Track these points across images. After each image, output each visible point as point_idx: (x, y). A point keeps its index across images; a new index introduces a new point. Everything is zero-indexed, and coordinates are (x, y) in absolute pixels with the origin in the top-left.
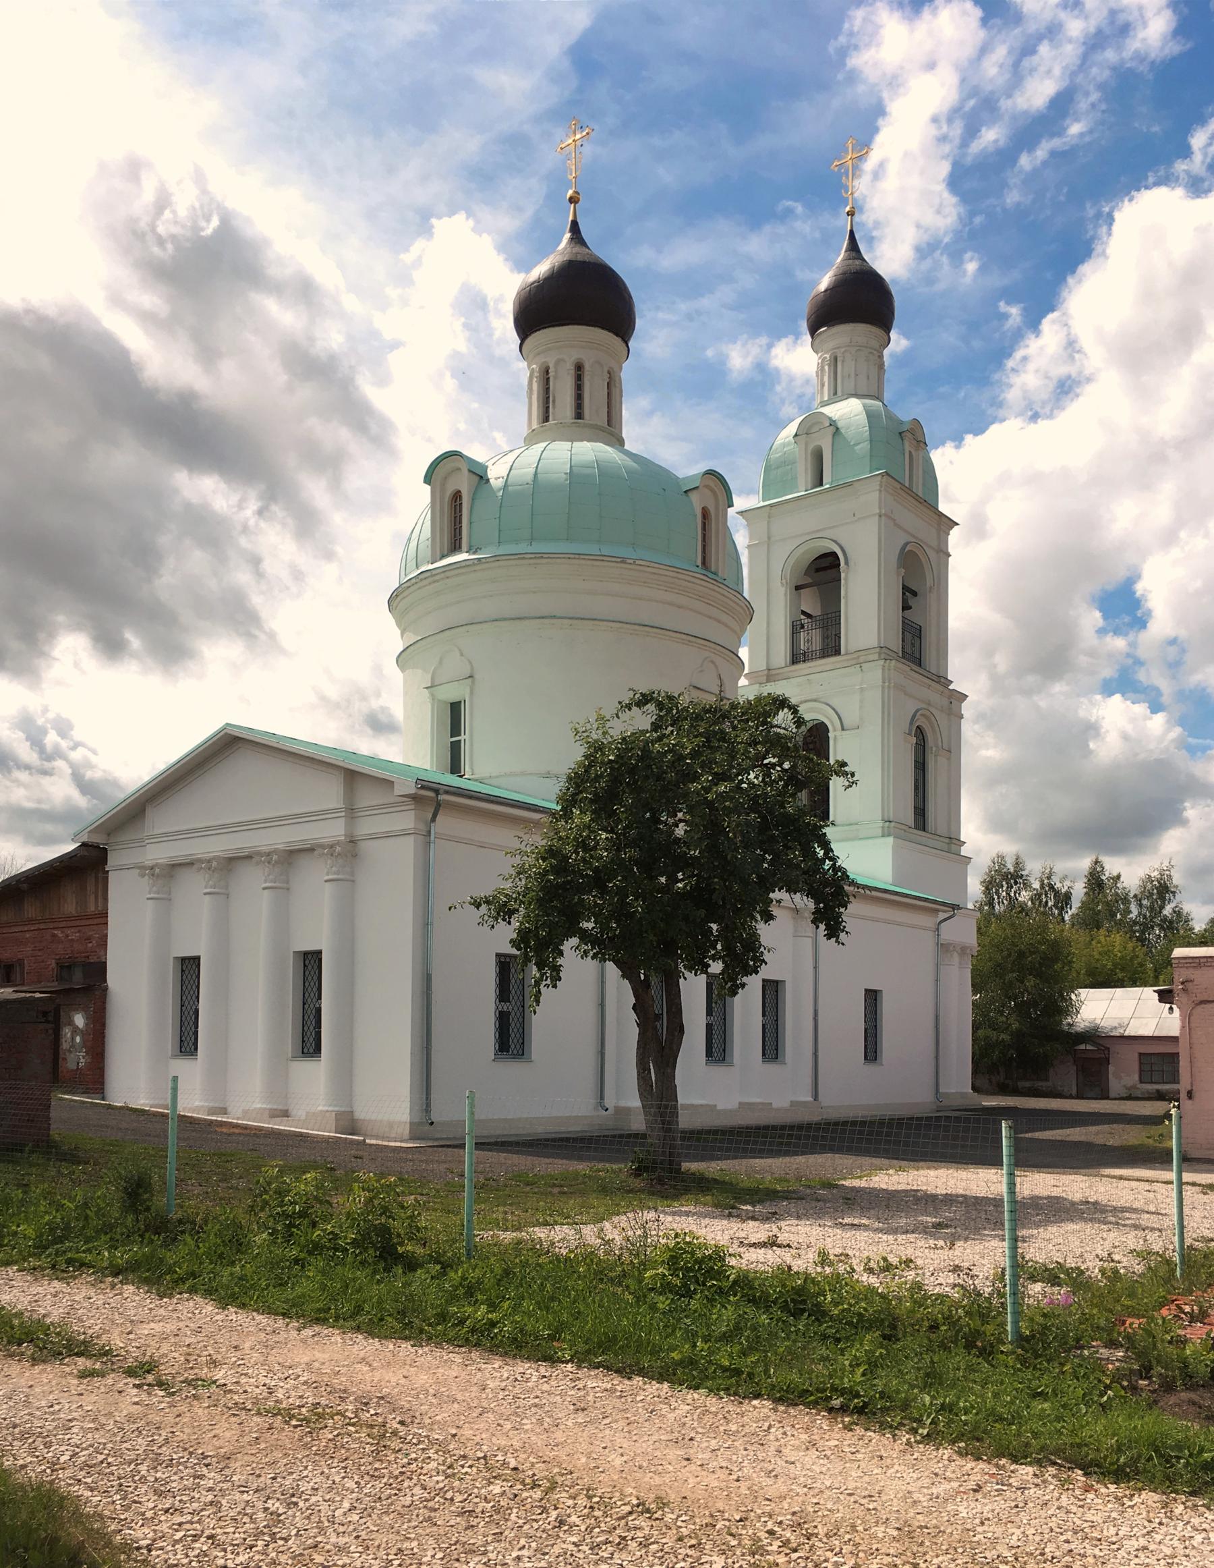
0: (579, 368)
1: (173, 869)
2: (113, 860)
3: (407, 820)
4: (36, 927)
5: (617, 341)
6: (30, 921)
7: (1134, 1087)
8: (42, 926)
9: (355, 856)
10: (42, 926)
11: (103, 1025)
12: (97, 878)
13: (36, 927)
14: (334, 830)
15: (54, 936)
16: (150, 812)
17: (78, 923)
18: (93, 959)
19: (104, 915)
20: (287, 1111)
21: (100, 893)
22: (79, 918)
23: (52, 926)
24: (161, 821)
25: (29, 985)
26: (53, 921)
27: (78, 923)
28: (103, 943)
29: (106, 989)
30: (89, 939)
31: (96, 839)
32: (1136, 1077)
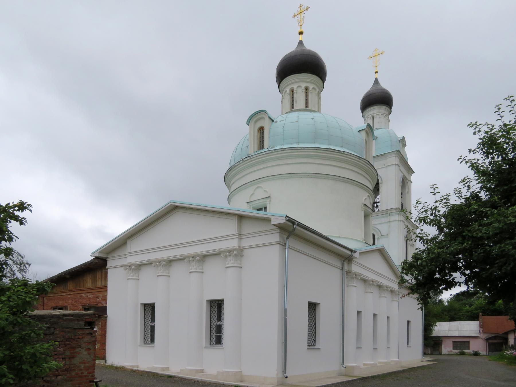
0: (307, 89)
1: (140, 266)
2: (110, 264)
3: (276, 237)
4: (73, 293)
5: (321, 82)
6: (70, 291)
7: (451, 351)
8: (76, 293)
9: (242, 256)
10: (76, 293)
11: (105, 332)
12: (102, 272)
13: (73, 293)
14: (233, 244)
15: (81, 296)
16: (129, 242)
17: (93, 291)
18: (100, 305)
19: (106, 287)
20: (203, 370)
21: (103, 279)
22: (93, 289)
23: (80, 292)
24: (133, 246)
25: (70, 310)
26: (81, 290)
27: (93, 291)
28: (105, 299)
29: (107, 317)
30: (98, 297)
31: (101, 255)
32: (452, 348)
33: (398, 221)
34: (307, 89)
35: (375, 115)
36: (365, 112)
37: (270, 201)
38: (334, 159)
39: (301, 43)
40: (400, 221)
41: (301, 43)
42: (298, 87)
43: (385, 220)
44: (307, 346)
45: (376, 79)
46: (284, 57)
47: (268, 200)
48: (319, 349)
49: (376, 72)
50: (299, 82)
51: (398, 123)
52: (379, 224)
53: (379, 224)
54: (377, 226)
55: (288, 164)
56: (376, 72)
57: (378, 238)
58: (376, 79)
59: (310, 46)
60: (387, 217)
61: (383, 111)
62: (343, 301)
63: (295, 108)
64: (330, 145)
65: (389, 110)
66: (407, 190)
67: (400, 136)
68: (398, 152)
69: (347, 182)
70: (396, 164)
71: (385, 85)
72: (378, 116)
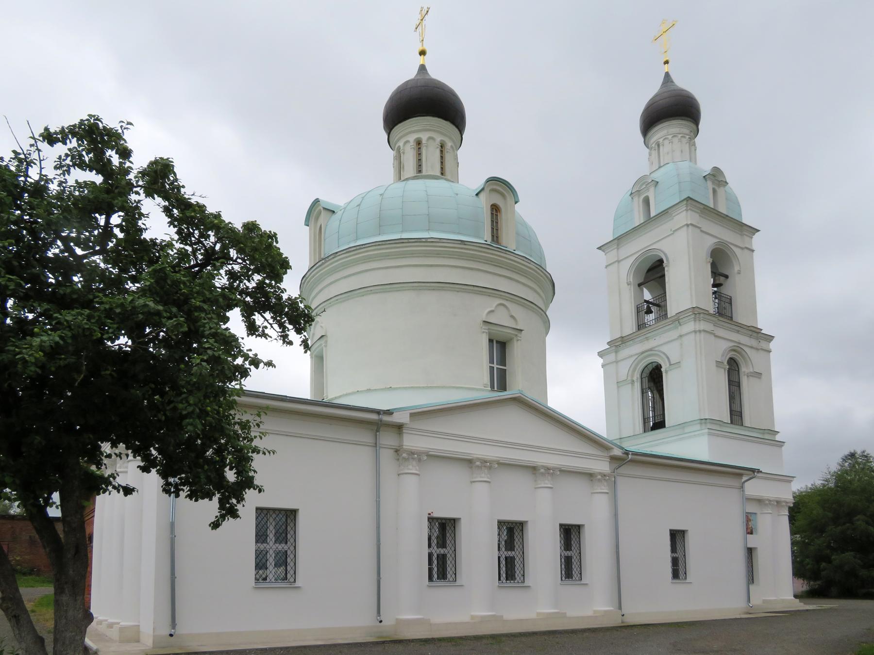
0: (419, 143)
33: (695, 332)
34: (419, 143)
35: (661, 140)
36: (650, 134)
37: (326, 342)
38: (413, 254)
39: (422, 68)
40: (700, 331)
41: (422, 68)
42: (430, 138)
43: (674, 334)
44: (254, 584)
45: (667, 75)
46: (392, 99)
47: (322, 341)
48: (299, 587)
49: (667, 62)
50: (424, 129)
51: (715, 142)
52: (665, 344)
53: (665, 344)
54: (661, 349)
55: (345, 277)
56: (667, 62)
57: (666, 372)
58: (667, 75)
59: (438, 73)
60: (676, 328)
61: (686, 131)
62: (616, 515)
63: (424, 173)
64: (433, 230)
65: (694, 126)
66: (736, 268)
67: (707, 169)
68: (690, 201)
69: (442, 289)
70: (687, 225)
71: (684, 82)
72: (666, 142)
